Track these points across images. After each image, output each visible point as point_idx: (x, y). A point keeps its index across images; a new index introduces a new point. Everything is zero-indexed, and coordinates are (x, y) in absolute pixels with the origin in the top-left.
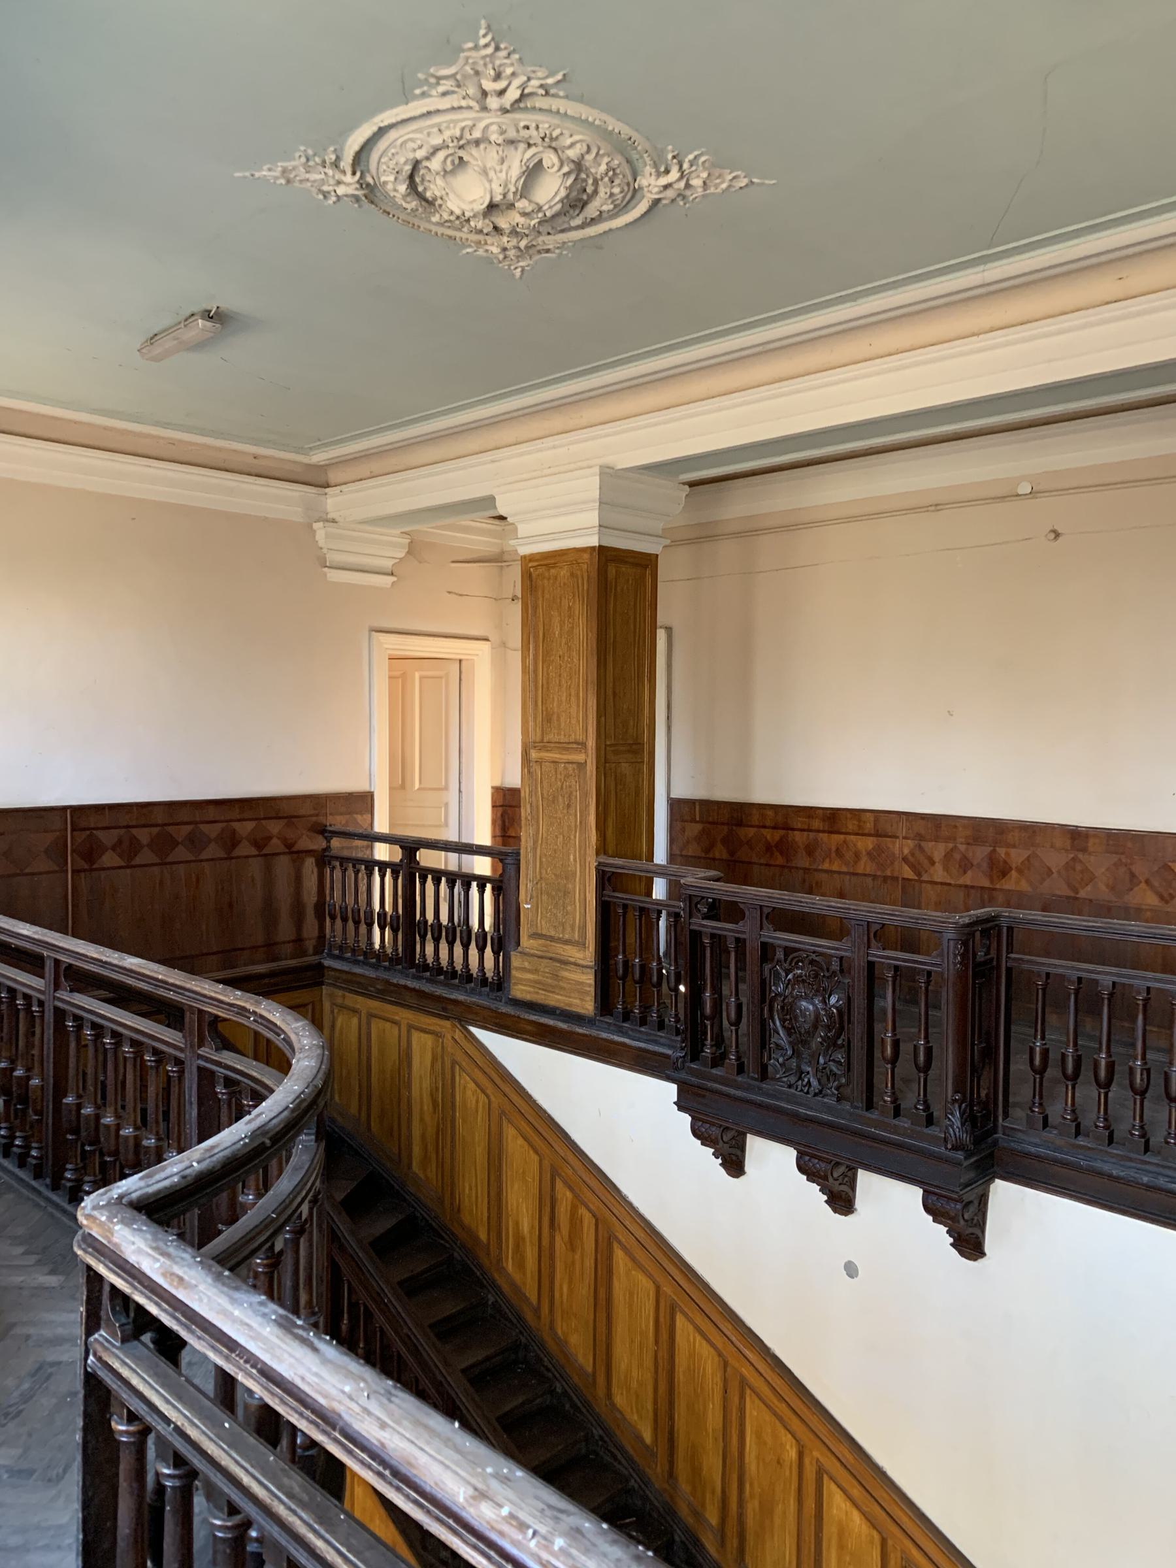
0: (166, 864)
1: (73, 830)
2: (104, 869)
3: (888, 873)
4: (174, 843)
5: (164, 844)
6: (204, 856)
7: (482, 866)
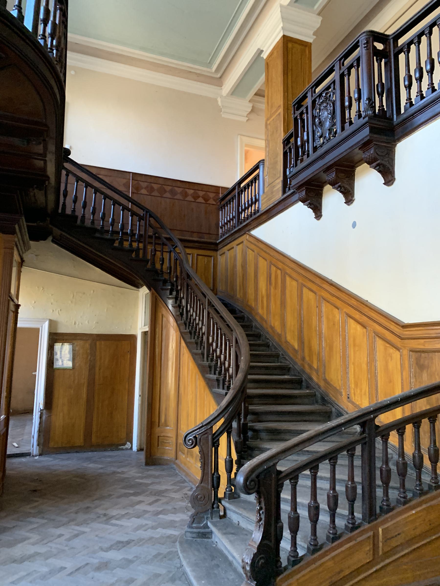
0: (162, 197)
1: (132, 180)
2: (141, 194)
3: (47, 139)
4: (165, 191)
5: (162, 191)
6: (175, 197)
7: (426, 478)
